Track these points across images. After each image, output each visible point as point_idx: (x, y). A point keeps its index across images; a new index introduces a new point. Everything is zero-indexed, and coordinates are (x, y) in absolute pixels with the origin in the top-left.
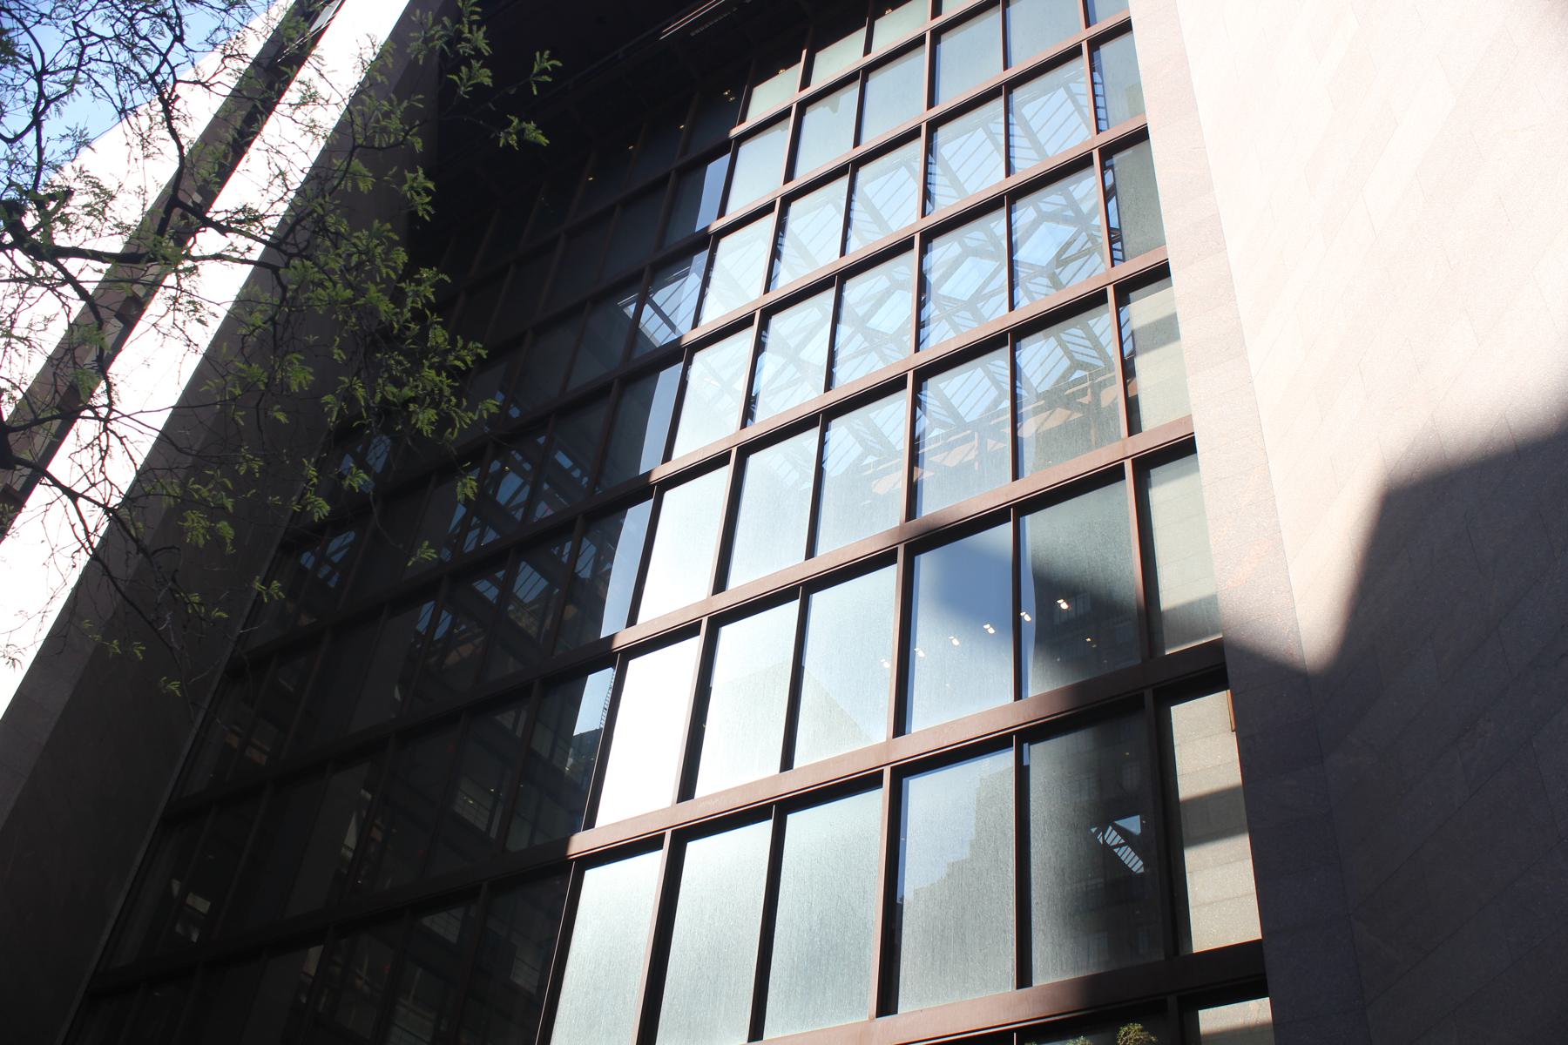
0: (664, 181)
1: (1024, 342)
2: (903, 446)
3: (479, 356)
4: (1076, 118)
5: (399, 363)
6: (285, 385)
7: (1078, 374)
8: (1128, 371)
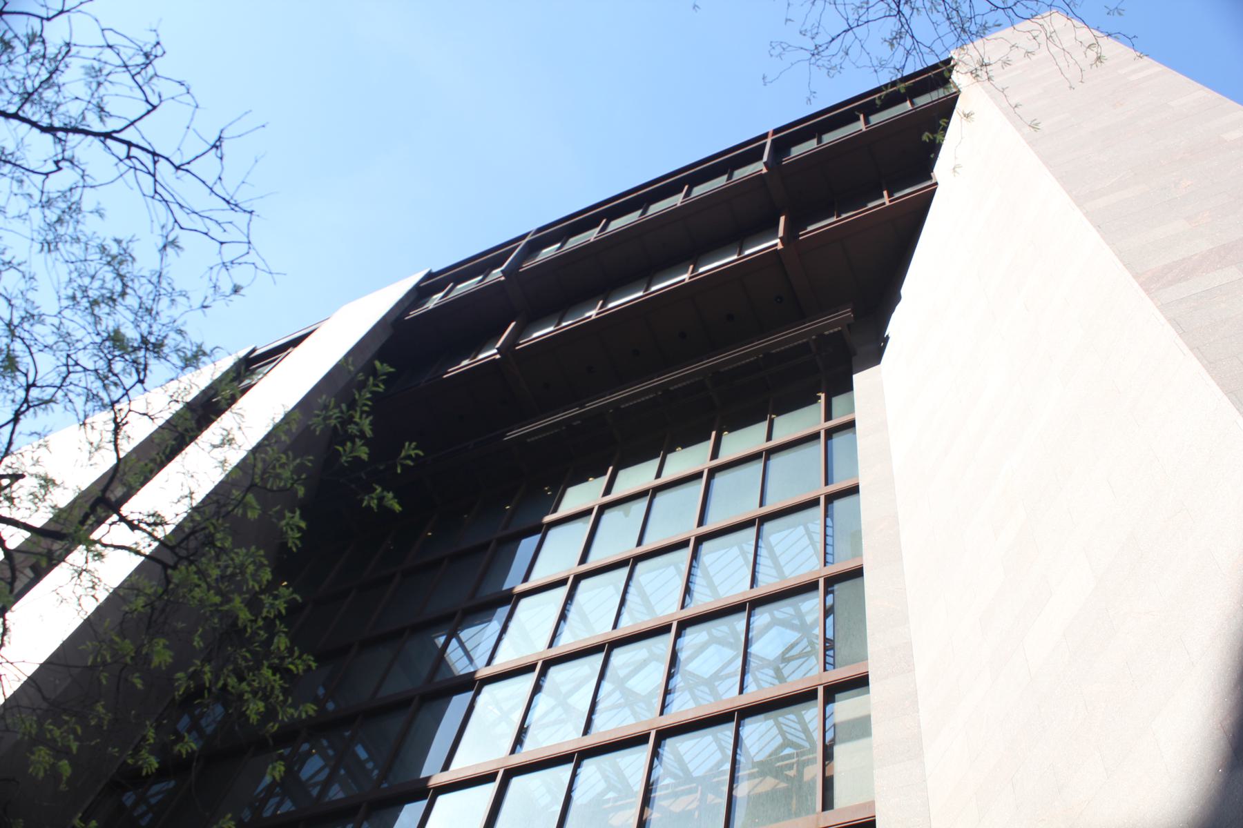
0: (484, 547)
1: (747, 721)
2: (639, 788)
3: (310, 666)
4: (810, 551)
5: (245, 658)
6: (147, 659)
7: (788, 751)
8: (828, 755)
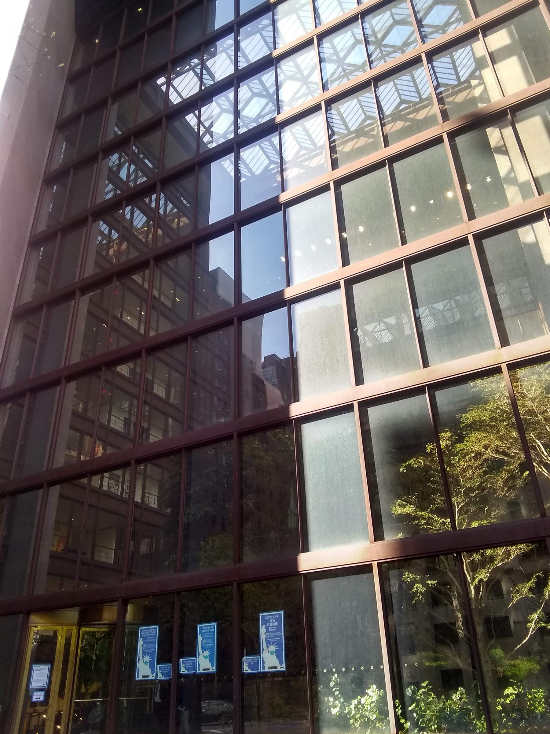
7: (303, 152)
